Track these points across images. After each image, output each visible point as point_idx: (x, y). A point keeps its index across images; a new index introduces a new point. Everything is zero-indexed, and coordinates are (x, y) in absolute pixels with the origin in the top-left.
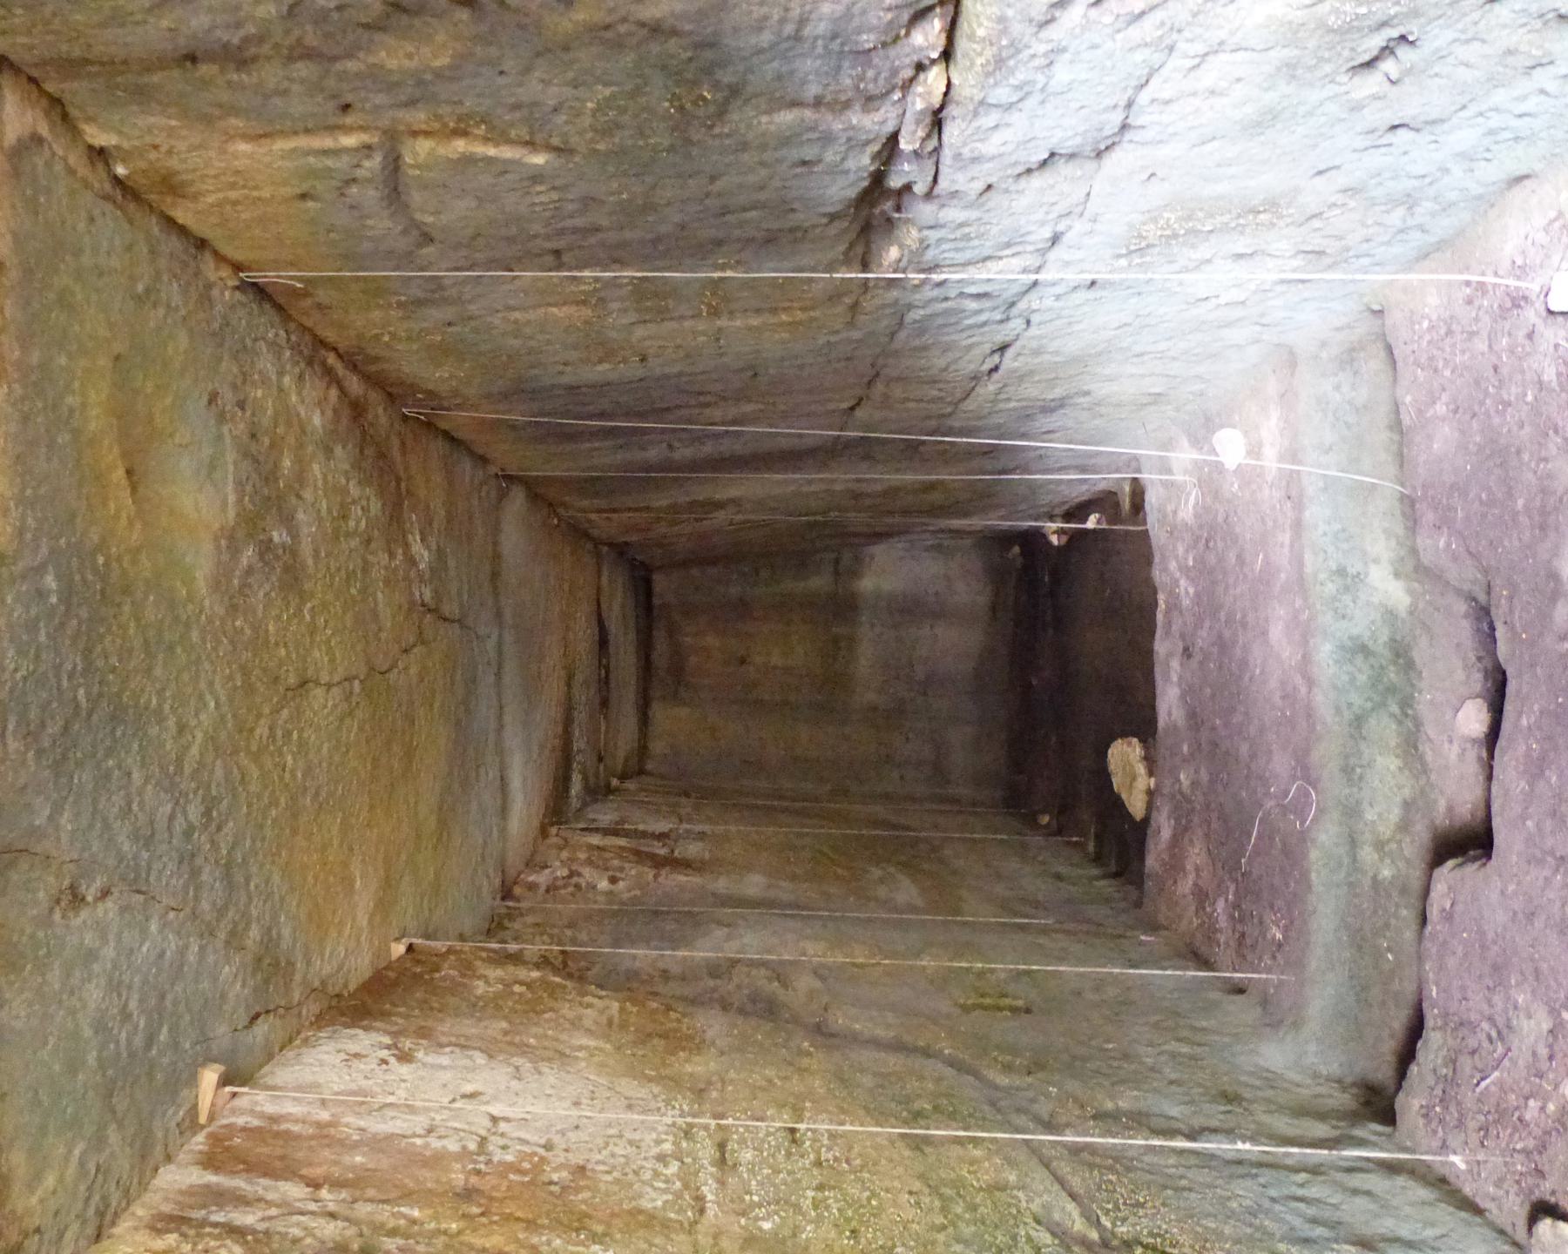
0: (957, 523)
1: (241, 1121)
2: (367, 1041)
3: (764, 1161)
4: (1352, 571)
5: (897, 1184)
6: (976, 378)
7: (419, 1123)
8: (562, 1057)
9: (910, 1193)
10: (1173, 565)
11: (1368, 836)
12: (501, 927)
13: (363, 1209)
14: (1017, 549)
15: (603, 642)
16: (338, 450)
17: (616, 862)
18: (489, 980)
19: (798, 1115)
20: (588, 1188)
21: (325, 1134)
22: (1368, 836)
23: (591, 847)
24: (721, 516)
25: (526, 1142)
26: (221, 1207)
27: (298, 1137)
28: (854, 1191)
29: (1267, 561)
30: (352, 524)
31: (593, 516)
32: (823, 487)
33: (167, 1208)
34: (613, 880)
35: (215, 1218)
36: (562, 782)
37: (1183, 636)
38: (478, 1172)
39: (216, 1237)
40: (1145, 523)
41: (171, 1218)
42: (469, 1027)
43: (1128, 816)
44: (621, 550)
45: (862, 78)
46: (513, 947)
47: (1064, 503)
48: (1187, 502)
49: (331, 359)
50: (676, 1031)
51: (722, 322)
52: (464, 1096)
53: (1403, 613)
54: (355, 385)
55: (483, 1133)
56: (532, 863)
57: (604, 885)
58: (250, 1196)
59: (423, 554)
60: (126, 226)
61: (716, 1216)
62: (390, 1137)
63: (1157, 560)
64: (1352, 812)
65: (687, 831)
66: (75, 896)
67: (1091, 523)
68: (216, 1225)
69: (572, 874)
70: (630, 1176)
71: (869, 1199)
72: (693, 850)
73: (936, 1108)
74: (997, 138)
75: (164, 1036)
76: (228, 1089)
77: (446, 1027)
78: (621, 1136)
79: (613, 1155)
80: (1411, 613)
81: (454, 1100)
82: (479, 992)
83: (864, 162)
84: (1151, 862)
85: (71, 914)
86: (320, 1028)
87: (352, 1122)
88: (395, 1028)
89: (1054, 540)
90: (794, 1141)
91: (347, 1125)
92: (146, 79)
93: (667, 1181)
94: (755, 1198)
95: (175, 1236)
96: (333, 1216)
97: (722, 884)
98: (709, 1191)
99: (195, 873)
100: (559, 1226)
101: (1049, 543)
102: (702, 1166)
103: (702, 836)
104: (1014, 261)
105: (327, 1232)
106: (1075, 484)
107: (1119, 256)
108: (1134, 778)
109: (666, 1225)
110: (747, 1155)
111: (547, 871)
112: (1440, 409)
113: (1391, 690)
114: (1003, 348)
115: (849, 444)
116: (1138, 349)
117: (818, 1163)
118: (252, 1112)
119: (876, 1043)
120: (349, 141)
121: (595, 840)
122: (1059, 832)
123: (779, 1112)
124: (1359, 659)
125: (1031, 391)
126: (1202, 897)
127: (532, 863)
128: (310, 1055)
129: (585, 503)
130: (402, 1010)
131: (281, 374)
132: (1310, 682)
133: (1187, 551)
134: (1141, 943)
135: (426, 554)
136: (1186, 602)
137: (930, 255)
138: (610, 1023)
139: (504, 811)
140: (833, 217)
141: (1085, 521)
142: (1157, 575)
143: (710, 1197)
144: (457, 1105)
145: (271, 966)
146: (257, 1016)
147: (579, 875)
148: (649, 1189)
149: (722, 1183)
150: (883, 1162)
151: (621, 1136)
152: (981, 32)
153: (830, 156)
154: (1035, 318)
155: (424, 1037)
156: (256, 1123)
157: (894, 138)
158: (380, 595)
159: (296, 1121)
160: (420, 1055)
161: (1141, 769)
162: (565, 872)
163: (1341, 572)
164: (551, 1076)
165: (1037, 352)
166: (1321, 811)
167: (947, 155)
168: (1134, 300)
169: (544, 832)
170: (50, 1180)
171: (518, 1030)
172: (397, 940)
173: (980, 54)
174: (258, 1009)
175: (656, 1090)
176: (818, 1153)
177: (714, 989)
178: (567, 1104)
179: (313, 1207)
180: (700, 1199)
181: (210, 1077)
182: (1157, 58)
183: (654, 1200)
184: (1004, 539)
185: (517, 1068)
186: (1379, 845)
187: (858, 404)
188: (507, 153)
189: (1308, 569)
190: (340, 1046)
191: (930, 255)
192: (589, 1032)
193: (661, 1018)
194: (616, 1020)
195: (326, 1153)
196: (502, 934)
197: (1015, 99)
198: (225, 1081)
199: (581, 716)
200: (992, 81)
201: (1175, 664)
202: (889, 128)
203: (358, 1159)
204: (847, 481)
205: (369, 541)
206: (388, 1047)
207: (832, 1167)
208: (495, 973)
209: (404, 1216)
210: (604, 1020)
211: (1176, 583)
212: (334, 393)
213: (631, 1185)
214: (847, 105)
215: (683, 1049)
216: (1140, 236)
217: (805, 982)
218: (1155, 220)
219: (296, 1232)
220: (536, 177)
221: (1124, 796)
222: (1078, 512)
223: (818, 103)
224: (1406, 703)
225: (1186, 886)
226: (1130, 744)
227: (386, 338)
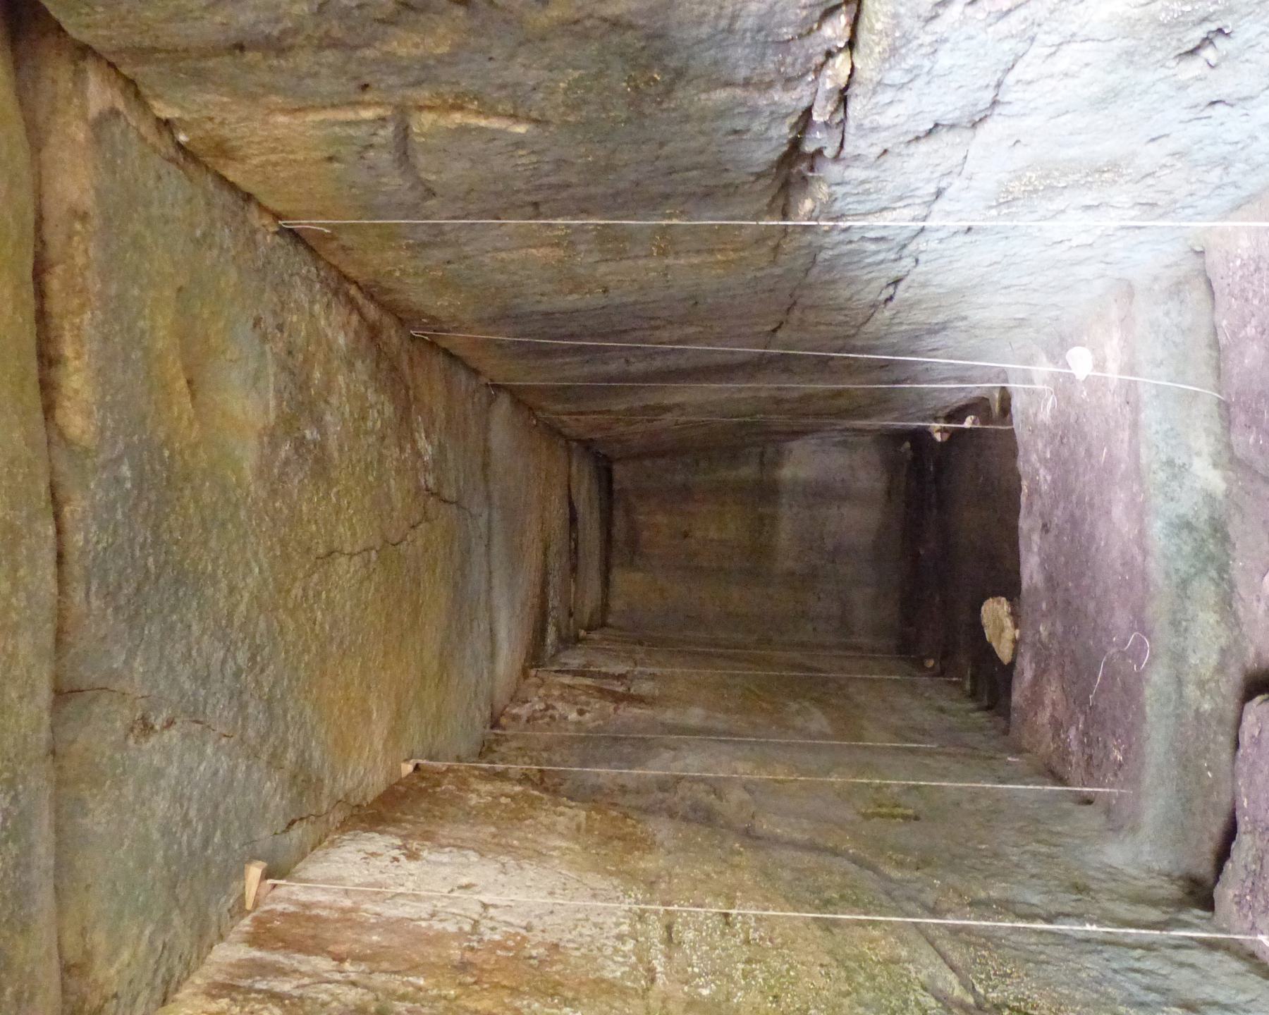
0: (859, 423)
1: (280, 907)
2: (381, 842)
4: (1178, 462)
6: (874, 306)
7: (425, 908)
8: (540, 856)
9: (822, 965)
10: (1034, 458)
11: (1191, 677)
13: (379, 979)
14: (907, 445)
15: (573, 520)
16: (359, 364)
17: (583, 698)
18: (480, 794)
20: (561, 961)
21: (348, 918)
22: (1191, 677)
23: (563, 686)
24: (668, 418)
26: (263, 976)
27: (326, 920)
28: (776, 964)
29: (1110, 455)
30: (370, 424)
31: (565, 418)
32: (751, 394)
33: (220, 978)
34: (581, 713)
35: (258, 986)
36: (539, 633)
37: (1042, 515)
38: (472, 949)
39: (260, 1001)
41: (223, 986)
42: (464, 831)
43: (998, 660)
44: (587, 445)
45: (782, 63)
46: (500, 767)
49: (353, 291)
50: (632, 834)
51: (669, 261)
52: (460, 887)
53: (1220, 497)
54: (372, 312)
55: (476, 917)
56: (516, 698)
57: (573, 716)
59: (427, 448)
60: (187, 183)
61: (664, 984)
62: (400, 921)
63: (1021, 453)
64: (1179, 657)
65: (641, 673)
66: (145, 725)
67: (968, 423)
68: (259, 991)
69: (547, 708)
71: (788, 971)
72: (646, 688)
73: (842, 897)
74: (892, 112)
75: (217, 838)
76: (270, 881)
77: (445, 831)
78: (587, 920)
79: (581, 935)
80: (1227, 496)
81: (452, 891)
82: (473, 803)
83: (784, 131)
84: (1016, 698)
85: (142, 740)
86: (344, 832)
87: (370, 908)
88: (404, 833)
89: (938, 437)
90: (727, 924)
91: (366, 911)
92: (202, 64)
93: (624, 956)
94: (696, 970)
95: (227, 1000)
96: (354, 984)
97: (669, 716)
98: (659, 964)
99: (243, 707)
101: (934, 440)
102: (653, 944)
103: (653, 677)
106: (955, 392)
108: (1002, 630)
109: (624, 992)
110: (690, 935)
111: (528, 705)
112: (1250, 331)
113: (1211, 558)
114: (896, 282)
115: (772, 360)
116: (1005, 282)
118: (289, 900)
119: (794, 844)
120: (368, 114)
121: (567, 680)
122: (942, 673)
124: (1185, 533)
125: (919, 316)
126: (1057, 726)
127: (516, 698)
128: (335, 854)
129: (559, 407)
130: (410, 817)
131: (312, 302)
132: (1145, 552)
133: (1045, 446)
134: (1008, 763)
135: (430, 448)
136: (1045, 487)
137: (837, 206)
138: (578, 828)
139: (492, 656)
140: (759, 176)
141: (962, 421)
142: (1021, 465)
143: (659, 969)
145: (304, 782)
146: (293, 822)
148: (610, 963)
149: (669, 957)
150: (800, 940)
151: (587, 920)
153: (756, 126)
154: (922, 258)
155: (427, 839)
156: (292, 909)
157: (808, 112)
158: (392, 482)
159: (325, 908)
160: (425, 854)
161: (1008, 622)
162: (542, 706)
163: (1170, 463)
164: (531, 871)
165: (924, 285)
166: (1154, 656)
167: (851, 126)
168: (1003, 243)
169: (525, 674)
170: (125, 956)
171: (504, 834)
172: (406, 761)
174: (293, 816)
175: (616, 882)
176: (747, 933)
177: (663, 800)
178: (544, 893)
180: (651, 970)
182: (1021, 47)
183: (614, 972)
184: (898, 436)
186: (1201, 684)
187: (779, 327)
188: (495, 123)
189: (1144, 461)
190: (360, 847)
191: (837, 206)
192: (561, 835)
193: (619, 823)
194: (583, 826)
196: (491, 756)
197: (906, 80)
198: (267, 875)
199: (555, 580)
200: (887, 65)
201: (1036, 537)
202: (805, 103)
203: (375, 938)
205: (383, 438)
206: (399, 848)
208: (485, 787)
209: (412, 984)
212: (355, 318)
213: (595, 959)
214: (770, 85)
215: (638, 849)
216: (1007, 191)
217: (736, 795)
218: (1019, 178)
219: (324, 997)
220: (519, 143)
221: (994, 644)
222: (957, 414)
223: (747, 83)
224: (1223, 569)
225: (1044, 717)
226: (999, 602)
227: (397, 274)
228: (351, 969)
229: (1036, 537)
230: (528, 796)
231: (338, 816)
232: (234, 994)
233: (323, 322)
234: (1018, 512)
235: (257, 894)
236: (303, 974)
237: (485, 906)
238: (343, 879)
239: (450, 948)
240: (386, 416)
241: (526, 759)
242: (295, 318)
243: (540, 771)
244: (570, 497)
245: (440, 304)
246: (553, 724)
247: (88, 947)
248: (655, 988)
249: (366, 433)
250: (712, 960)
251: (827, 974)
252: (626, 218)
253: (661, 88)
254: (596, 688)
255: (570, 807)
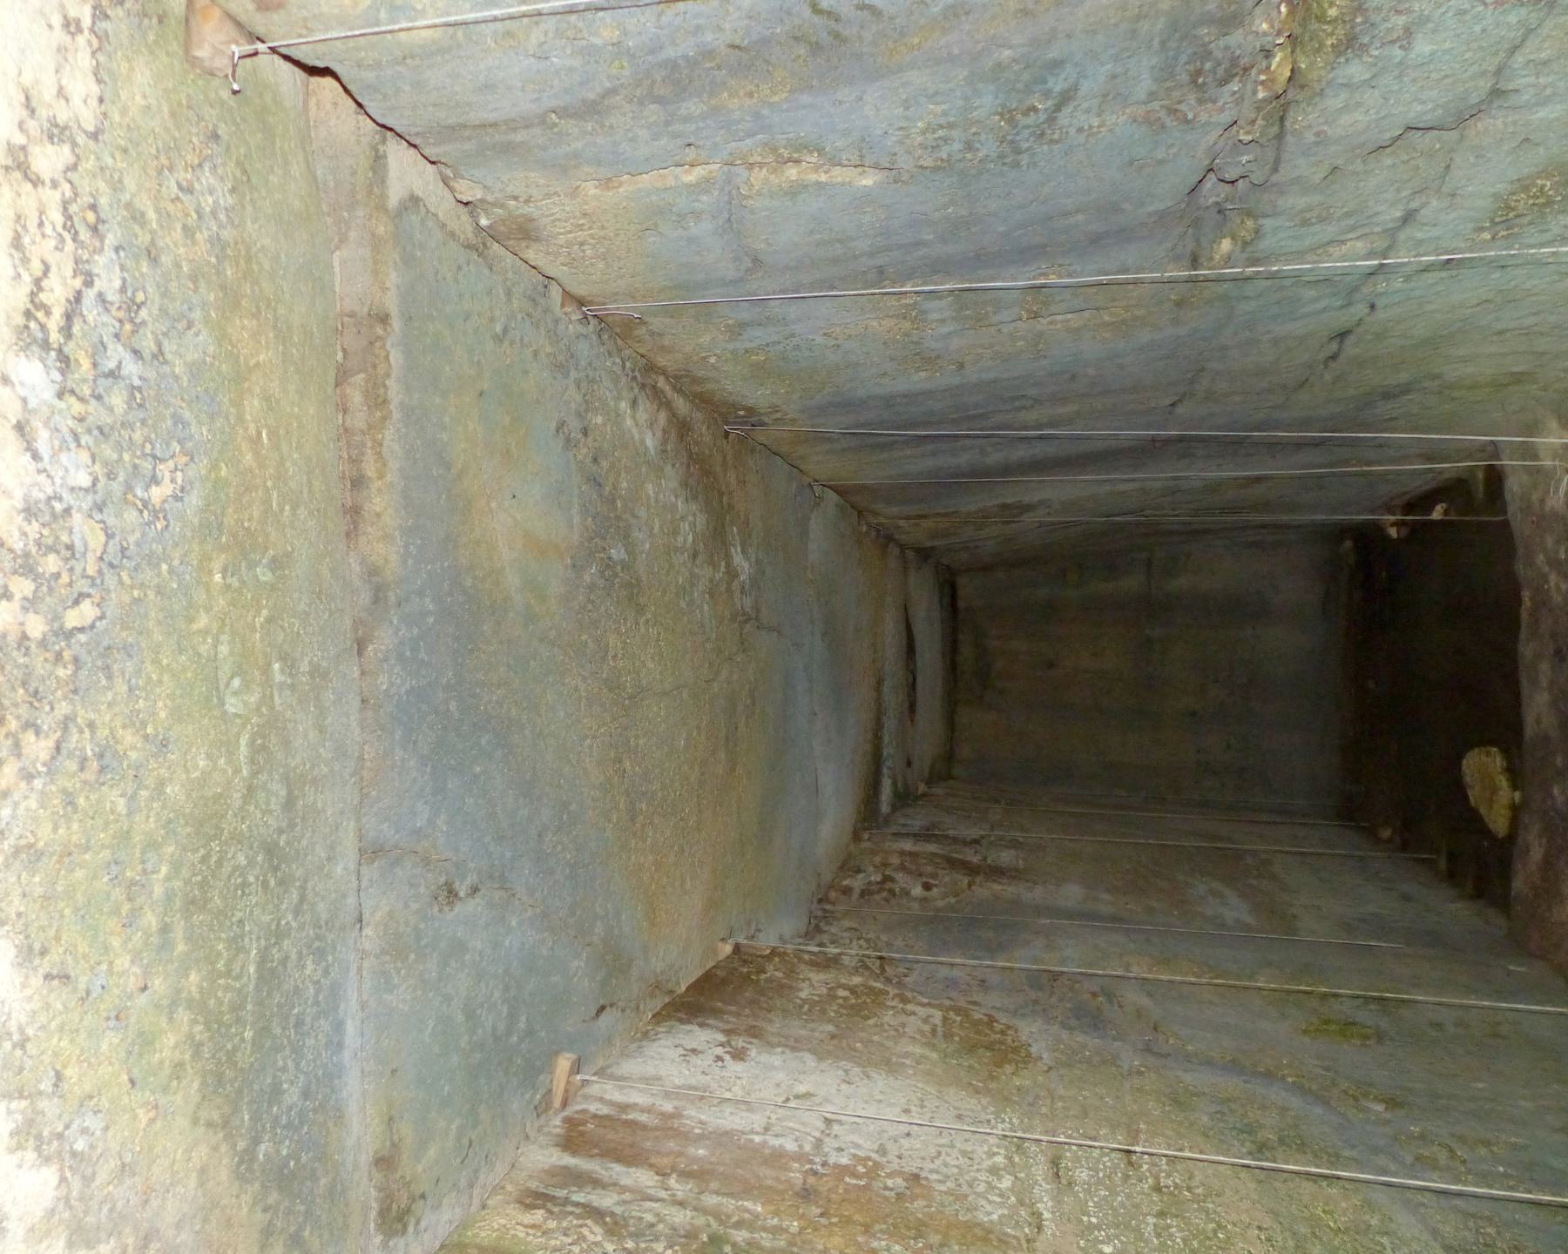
1: (593, 1107)
2: (701, 1036)
3: (1099, 1182)
5: (1244, 1217)
7: (758, 1121)
8: (890, 1066)
9: (1259, 1228)
10: (1540, 558)
12: (818, 929)
13: (711, 1200)
14: (1348, 544)
17: (929, 869)
18: (812, 984)
19: (1134, 1137)
20: (924, 1197)
21: (669, 1126)
23: (902, 853)
24: (1028, 518)
25: (857, 1146)
26: (581, 1188)
27: (644, 1127)
28: (1198, 1220)
30: (680, 539)
31: (902, 523)
32: (1137, 485)
33: (533, 1185)
34: (927, 887)
35: (575, 1198)
36: (873, 786)
38: (815, 1173)
39: (578, 1217)
40: (1505, 513)
41: (538, 1195)
42: (797, 1028)
43: (1486, 832)
44: (924, 554)
46: (832, 950)
47: (1405, 493)
48: (1557, 488)
49: (661, 382)
50: (1002, 1043)
52: (797, 1097)
54: (681, 405)
55: (817, 1134)
56: (848, 866)
57: (917, 891)
58: (606, 1180)
60: (486, 271)
61: (1053, 1235)
63: (1521, 551)
65: (1001, 838)
66: (450, 892)
67: (1437, 514)
68: (577, 1204)
69: (887, 879)
70: (965, 1187)
71: (1215, 1232)
72: (1006, 857)
73: (1282, 1141)
77: (775, 1025)
78: (953, 1146)
79: (946, 1165)
81: (788, 1100)
82: (803, 995)
84: (1518, 884)
85: (446, 909)
86: (658, 1024)
87: (695, 1116)
88: (729, 1027)
90: (1130, 1163)
91: (690, 1118)
92: (512, 137)
93: (1001, 1195)
94: (1094, 1220)
95: (542, 1212)
96: (681, 1204)
97: (1035, 894)
98: (1045, 1207)
100: (894, 1233)
101: (1387, 538)
102: (1036, 1183)
103: (1014, 844)
104: (1359, 244)
105: (676, 1220)
106: (1415, 473)
107: (1482, 229)
108: (1495, 791)
109: (1004, 1242)
110: (1083, 1175)
111: (861, 876)
114: (1343, 335)
115: (1168, 441)
116: (1499, 326)
117: (1157, 1189)
118: (601, 1100)
121: (908, 845)
122: (1405, 846)
123: (1113, 1133)
128: (652, 1049)
129: (895, 510)
130: (733, 1008)
131: (619, 398)
133: (1558, 542)
134: (1509, 973)
135: (746, 565)
138: (934, 1032)
141: (1429, 510)
142: (1520, 568)
143: (1046, 1215)
144: (792, 1104)
146: (603, 1008)
147: (892, 880)
148: (983, 1202)
149: (1058, 1201)
150: (1228, 1192)
151: (953, 1146)
152: (1333, 12)
154: (1380, 303)
155: (755, 1036)
156: (605, 1111)
158: (706, 607)
159: (643, 1111)
160: (753, 1053)
161: (1503, 782)
162: (879, 878)
164: (880, 1081)
168: (1497, 275)
169: (856, 837)
170: (432, 1152)
173: (1332, 34)
174: (602, 1002)
175: (984, 1101)
176: (1157, 1178)
178: (898, 1110)
179: (663, 1194)
180: (1037, 1215)
181: (564, 1063)
185: (846, 1071)
187: (1180, 401)
190: (677, 1042)
194: (940, 1030)
195: (671, 1144)
196: (818, 939)
197: (1367, 76)
199: (890, 724)
200: (1342, 60)
201: (1544, 666)
203: (701, 1152)
204: (1166, 479)
205: (695, 556)
206: (722, 1045)
207: (1171, 1194)
208: (817, 977)
209: (748, 1211)
210: (927, 1028)
211: (1545, 578)
213: (966, 1196)
215: (1010, 1062)
216: (1509, 208)
218: (1526, 189)
219: (649, 1217)
221: (1483, 811)
222: (1424, 501)
226: (1488, 754)
227: (713, 360)
228: (677, 1186)
229: (1544, 666)
230: (872, 989)
231: (658, 1003)
232: (549, 1205)
233: (629, 422)
234: (1519, 628)
235: (566, 1091)
236: (624, 1189)
237: (828, 1122)
238: (660, 1079)
239: (791, 1170)
240: (699, 527)
241: (862, 942)
242: (599, 420)
243: (881, 958)
244: (907, 620)
245: (759, 396)
246: (893, 901)
247: (396, 1137)
248: (1042, 1237)
249: (676, 550)
250: (1112, 1208)
251: (1269, 1240)
252: (993, 279)
253: (1043, 117)
254: (942, 856)
255: (923, 1005)
